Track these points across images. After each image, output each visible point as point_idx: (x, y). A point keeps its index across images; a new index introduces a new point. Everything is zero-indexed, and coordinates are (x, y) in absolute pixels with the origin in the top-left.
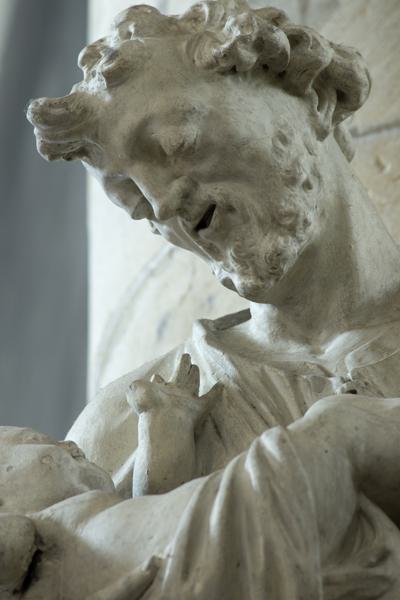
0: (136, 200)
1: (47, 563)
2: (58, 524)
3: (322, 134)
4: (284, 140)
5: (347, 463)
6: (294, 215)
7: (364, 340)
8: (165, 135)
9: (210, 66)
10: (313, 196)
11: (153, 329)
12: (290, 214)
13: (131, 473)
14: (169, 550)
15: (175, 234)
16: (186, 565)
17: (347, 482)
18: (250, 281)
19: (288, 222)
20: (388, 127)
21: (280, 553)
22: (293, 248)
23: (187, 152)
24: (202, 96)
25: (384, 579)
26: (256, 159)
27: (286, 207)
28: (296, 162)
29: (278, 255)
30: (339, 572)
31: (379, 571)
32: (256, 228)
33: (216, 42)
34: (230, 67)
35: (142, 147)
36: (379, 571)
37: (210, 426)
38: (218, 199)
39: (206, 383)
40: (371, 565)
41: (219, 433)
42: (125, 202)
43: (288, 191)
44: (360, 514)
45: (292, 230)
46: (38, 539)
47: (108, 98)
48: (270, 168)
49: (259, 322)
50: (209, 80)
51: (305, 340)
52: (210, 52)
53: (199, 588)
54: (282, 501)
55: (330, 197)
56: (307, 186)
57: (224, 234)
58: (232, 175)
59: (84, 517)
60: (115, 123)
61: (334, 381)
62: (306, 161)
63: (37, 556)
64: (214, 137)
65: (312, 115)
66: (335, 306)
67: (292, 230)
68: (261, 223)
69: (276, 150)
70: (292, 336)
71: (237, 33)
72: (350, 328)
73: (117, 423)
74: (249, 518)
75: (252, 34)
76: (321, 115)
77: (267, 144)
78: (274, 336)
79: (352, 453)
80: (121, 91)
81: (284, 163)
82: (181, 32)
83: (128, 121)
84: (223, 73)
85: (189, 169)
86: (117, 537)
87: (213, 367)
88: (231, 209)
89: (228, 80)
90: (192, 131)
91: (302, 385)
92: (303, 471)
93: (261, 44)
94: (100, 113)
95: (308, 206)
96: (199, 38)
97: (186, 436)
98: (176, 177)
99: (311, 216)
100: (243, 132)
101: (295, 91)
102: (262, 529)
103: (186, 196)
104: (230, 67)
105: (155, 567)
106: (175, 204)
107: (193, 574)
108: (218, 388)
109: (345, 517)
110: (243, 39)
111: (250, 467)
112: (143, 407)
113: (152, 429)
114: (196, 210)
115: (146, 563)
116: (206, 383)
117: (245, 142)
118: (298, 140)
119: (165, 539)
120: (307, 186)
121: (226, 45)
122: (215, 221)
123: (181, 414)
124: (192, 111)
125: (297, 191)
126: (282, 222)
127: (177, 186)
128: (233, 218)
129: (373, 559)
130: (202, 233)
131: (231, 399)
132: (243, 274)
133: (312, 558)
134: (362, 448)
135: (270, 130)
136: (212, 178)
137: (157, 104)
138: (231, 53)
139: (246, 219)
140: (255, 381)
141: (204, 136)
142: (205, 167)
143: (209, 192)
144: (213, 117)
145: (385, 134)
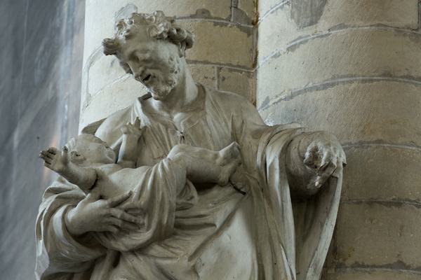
0: (128, 69)
1: (99, 183)
2: (103, 173)
3: (181, 56)
4: (172, 60)
5: (185, 172)
6: (172, 81)
7: (185, 117)
8: (140, 56)
9: (154, 37)
10: (177, 76)
11: (110, 64)
12: (170, 81)
13: (120, 145)
14: (136, 189)
15: (168, 146)
16: (140, 196)
17: (185, 177)
18: (157, 96)
19: (170, 83)
20: (185, 18)
21: (166, 196)
22: (169, 89)
23: (146, 61)
24: (151, 46)
25: (191, 204)
26: (164, 64)
27: (170, 79)
28: (174, 66)
29: (166, 91)
30: (180, 201)
31: (190, 202)
32: (161, 83)
33: (157, 30)
34: (160, 38)
35: (133, 57)
36: (190, 202)
37: (142, 139)
38: (152, 74)
39: (142, 124)
40: (188, 200)
41: (144, 141)
42: (125, 69)
43: (171, 74)
44: (187, 184)
45: (171, 85)
46: (97, 176)
47: (125, 42)
48: (167, 67)
49: (155, 103)
50: (154, 41)
51: (169, 112)
52: (154, 33)
53: (142, 203)
54: (168, 182)
55: (181, 75)
56: (176, 72)
57: (152, 83)
58: (156, 68)
59: (111, 172)
60: (126, 49)
61: (178, 132)
62: (177, 65)
63: (96, 180)
64: (153, 58)
65: (179, 50)
66: (178, 104)
67: (171, 85)
68: (163, 82)
69: (170, 63)
70: (165, 111)
71: (163, 29)
72: (182, 112)
73: (115, 129)
74: (158, 184)
75: (167, 30)
76: (181, 50)
77: (167, 61)
78: (160, 109)
79: (187, 169)
80: (129, 41)
81: (171, 66)
82: (147, 24)
83: (129, 50)
84: (158, 39)
85: (145, 65)
86: (120, 181)
87: (145, 120)
88: (154, 77)
89: (159, 41)
90: (147, 56)
91: (169, 131)
92: (174, 175)
93: (169, 33)
94: (122, 45)
95: (175, 78)
96: (152, 28)
97: (136, 142)
98: (141, 66)
99: (176, 81)
100: (161, 57)
101: (175, 43)
102: (161, 189)
103: (143, 72)
104: (160, 38)
105: (131, 194)
106: (139, 74)
107: (141, 199)
108: (145, 127)
109: (183, 186)
110: (164, 32)
111: (160, 170)
112: (125, 133)
113: (127, 139)
114: (145, 76)
115: (128, 192)
116: (142, 124)
117: (161, 61)
118: (175, 59)
119: (134, 186)
120: (176, 72)
121: (160, 33)
122: (150, 79)
123: (135, 136)
124: (148, 50)
125: (174, 74)
126: (167, 82)
127: (141, 69)
128: (155, 79)
129: (189, 198)
130: (145, 82)
131: (148, 131)
132: (155, 94)
133: (174, 199)
134: (190, 168)
135: (168, 56)
136: (151, 68)
137: (139, 47)
138: (161, 34)
139: (158, 80)
140: (156, 128)
141: (150, 57)
142: (149, 65)
143: (149, 71)
144: (154, 52)
145: (184, 20)
